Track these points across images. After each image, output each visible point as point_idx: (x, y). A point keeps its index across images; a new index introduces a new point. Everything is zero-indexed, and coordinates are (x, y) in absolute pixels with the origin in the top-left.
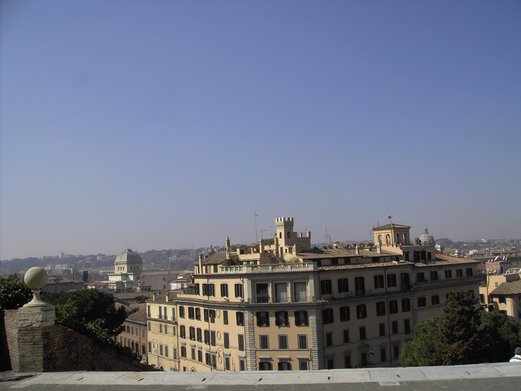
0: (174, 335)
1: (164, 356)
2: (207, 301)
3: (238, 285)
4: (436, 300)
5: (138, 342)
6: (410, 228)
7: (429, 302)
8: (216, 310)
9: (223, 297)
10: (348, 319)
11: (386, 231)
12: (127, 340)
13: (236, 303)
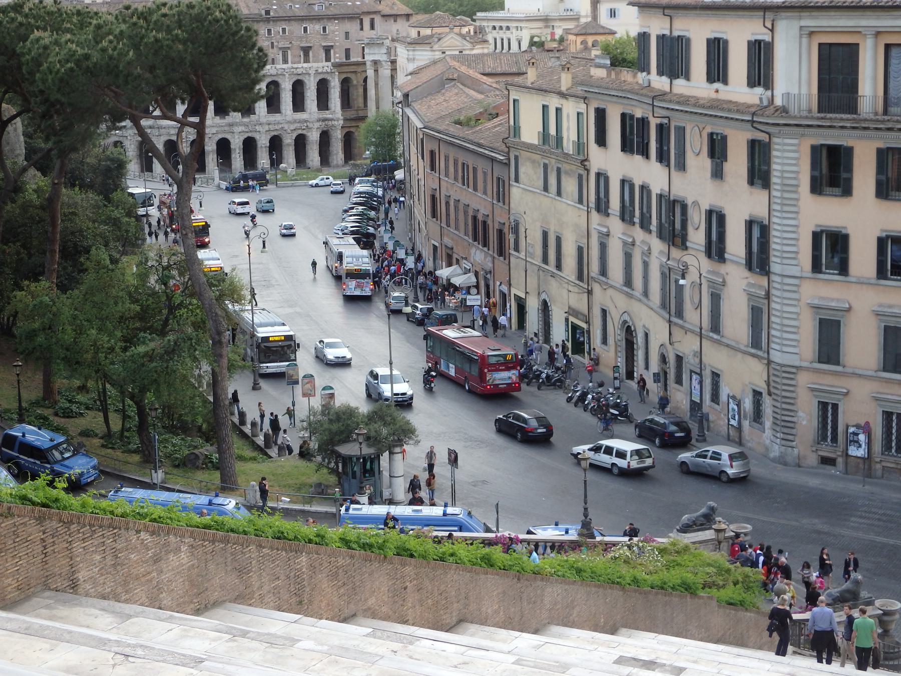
0: (580, 201)
1: (552, 267)
2: (664, 94)
3: (758, 42)
5: (488, 216)
8: (727, 132)
12: (461, 207)
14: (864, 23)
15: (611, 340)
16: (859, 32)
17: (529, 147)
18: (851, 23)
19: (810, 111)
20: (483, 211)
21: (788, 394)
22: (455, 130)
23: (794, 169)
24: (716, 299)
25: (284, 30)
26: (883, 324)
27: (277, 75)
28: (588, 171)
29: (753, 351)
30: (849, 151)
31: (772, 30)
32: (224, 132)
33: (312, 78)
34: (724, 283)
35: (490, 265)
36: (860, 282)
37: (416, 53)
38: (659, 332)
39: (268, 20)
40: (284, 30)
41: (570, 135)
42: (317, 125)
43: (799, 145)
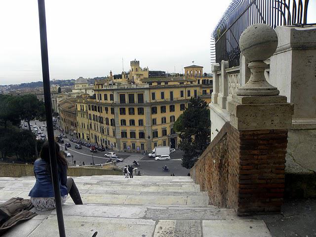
9: (279, 91)
10: (156, 113)
13: (110, 104)
22: (68, 109)
24: (108, 130)
36: (168, 123)
38: (99, 135)
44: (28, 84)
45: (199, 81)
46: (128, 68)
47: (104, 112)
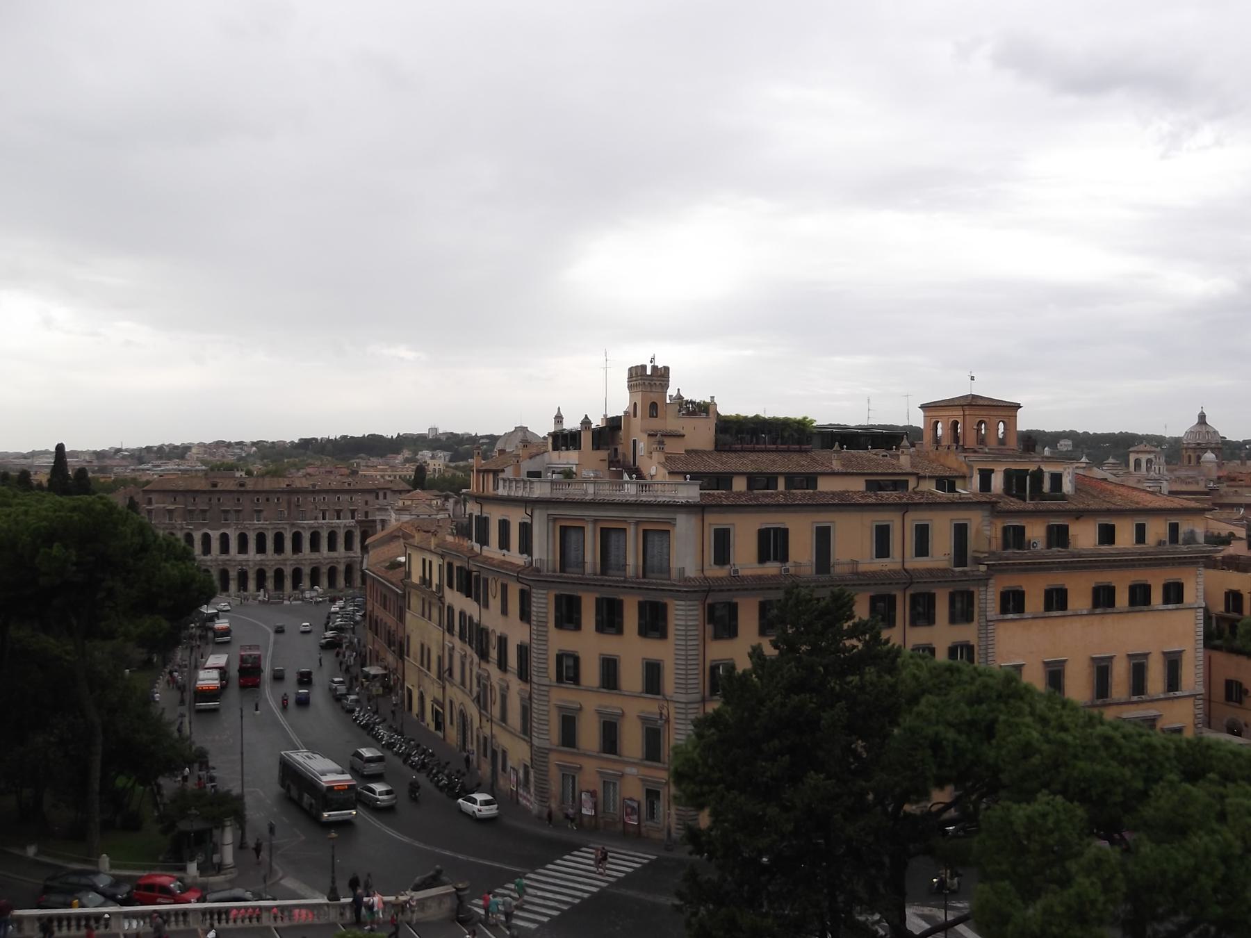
4: (1174, 593)
6: (1018, 406)
7: (1122, 599)
11: (950, 413)
14: (587, 513)
15: (455, 723)
16: (625, 521)
17: (415, 586)
18: (578, 513)
19: (554, 571)
20: (393, 629)
21: (543, 768)
23: (545, 610)
25: (324, 498)
26: (602, 720)
27: (318, 527)
28: (443, 604)
29: (523, 736)
30: (579, 599)
31: (531, 516)
32: (280, 564)
33: (342, 530)
34: (508, 687)
35: (395, 664)
36: (589, 690)
37: (401, 516)
39: (313, 492)
40: (324, 498)
41: (435, 580)
42: (343, 560)
43: (548, 594)
44: (329, 440)
45: (986, 476)
46: (619, 401)
47: (495, 603)
